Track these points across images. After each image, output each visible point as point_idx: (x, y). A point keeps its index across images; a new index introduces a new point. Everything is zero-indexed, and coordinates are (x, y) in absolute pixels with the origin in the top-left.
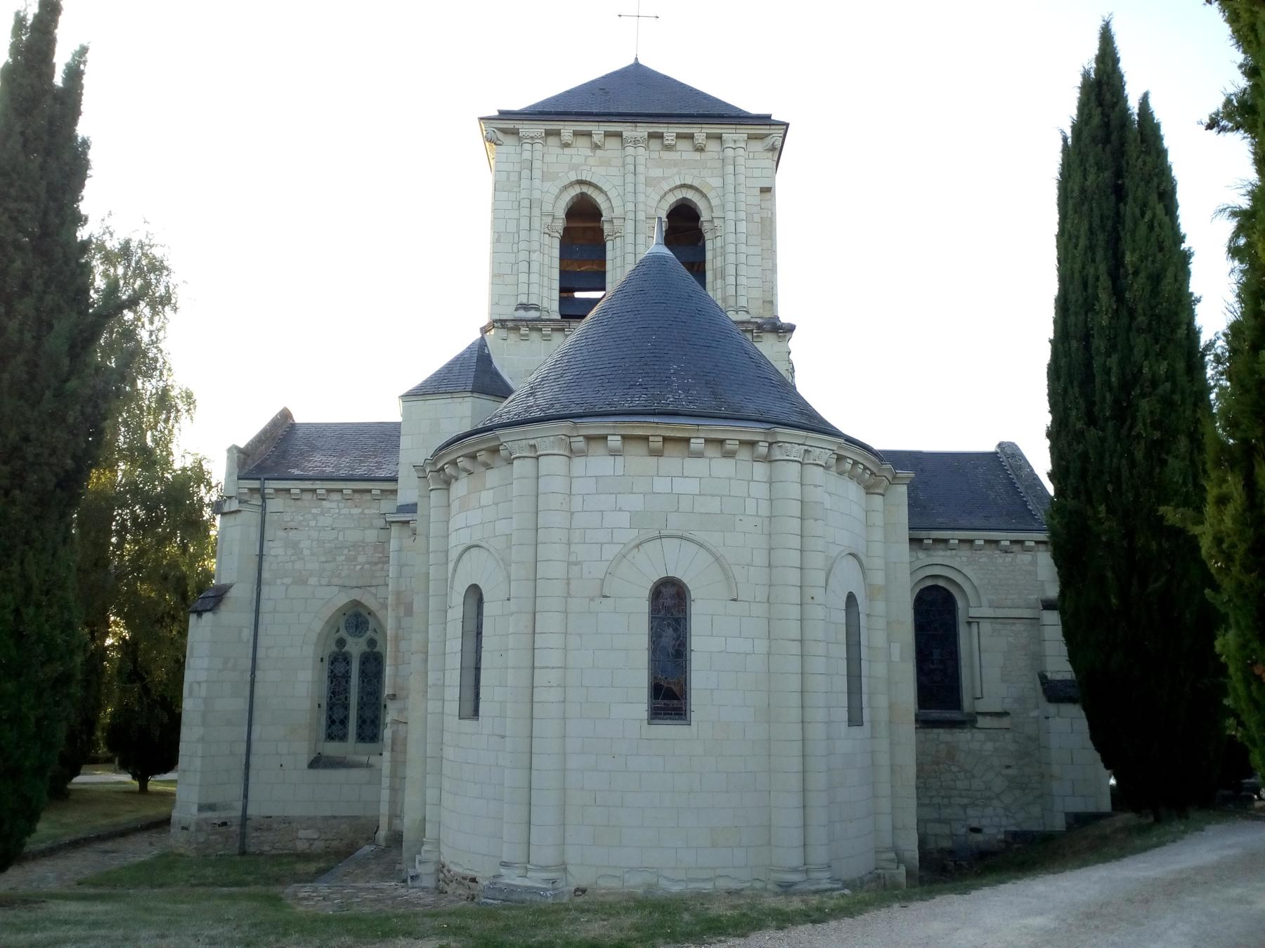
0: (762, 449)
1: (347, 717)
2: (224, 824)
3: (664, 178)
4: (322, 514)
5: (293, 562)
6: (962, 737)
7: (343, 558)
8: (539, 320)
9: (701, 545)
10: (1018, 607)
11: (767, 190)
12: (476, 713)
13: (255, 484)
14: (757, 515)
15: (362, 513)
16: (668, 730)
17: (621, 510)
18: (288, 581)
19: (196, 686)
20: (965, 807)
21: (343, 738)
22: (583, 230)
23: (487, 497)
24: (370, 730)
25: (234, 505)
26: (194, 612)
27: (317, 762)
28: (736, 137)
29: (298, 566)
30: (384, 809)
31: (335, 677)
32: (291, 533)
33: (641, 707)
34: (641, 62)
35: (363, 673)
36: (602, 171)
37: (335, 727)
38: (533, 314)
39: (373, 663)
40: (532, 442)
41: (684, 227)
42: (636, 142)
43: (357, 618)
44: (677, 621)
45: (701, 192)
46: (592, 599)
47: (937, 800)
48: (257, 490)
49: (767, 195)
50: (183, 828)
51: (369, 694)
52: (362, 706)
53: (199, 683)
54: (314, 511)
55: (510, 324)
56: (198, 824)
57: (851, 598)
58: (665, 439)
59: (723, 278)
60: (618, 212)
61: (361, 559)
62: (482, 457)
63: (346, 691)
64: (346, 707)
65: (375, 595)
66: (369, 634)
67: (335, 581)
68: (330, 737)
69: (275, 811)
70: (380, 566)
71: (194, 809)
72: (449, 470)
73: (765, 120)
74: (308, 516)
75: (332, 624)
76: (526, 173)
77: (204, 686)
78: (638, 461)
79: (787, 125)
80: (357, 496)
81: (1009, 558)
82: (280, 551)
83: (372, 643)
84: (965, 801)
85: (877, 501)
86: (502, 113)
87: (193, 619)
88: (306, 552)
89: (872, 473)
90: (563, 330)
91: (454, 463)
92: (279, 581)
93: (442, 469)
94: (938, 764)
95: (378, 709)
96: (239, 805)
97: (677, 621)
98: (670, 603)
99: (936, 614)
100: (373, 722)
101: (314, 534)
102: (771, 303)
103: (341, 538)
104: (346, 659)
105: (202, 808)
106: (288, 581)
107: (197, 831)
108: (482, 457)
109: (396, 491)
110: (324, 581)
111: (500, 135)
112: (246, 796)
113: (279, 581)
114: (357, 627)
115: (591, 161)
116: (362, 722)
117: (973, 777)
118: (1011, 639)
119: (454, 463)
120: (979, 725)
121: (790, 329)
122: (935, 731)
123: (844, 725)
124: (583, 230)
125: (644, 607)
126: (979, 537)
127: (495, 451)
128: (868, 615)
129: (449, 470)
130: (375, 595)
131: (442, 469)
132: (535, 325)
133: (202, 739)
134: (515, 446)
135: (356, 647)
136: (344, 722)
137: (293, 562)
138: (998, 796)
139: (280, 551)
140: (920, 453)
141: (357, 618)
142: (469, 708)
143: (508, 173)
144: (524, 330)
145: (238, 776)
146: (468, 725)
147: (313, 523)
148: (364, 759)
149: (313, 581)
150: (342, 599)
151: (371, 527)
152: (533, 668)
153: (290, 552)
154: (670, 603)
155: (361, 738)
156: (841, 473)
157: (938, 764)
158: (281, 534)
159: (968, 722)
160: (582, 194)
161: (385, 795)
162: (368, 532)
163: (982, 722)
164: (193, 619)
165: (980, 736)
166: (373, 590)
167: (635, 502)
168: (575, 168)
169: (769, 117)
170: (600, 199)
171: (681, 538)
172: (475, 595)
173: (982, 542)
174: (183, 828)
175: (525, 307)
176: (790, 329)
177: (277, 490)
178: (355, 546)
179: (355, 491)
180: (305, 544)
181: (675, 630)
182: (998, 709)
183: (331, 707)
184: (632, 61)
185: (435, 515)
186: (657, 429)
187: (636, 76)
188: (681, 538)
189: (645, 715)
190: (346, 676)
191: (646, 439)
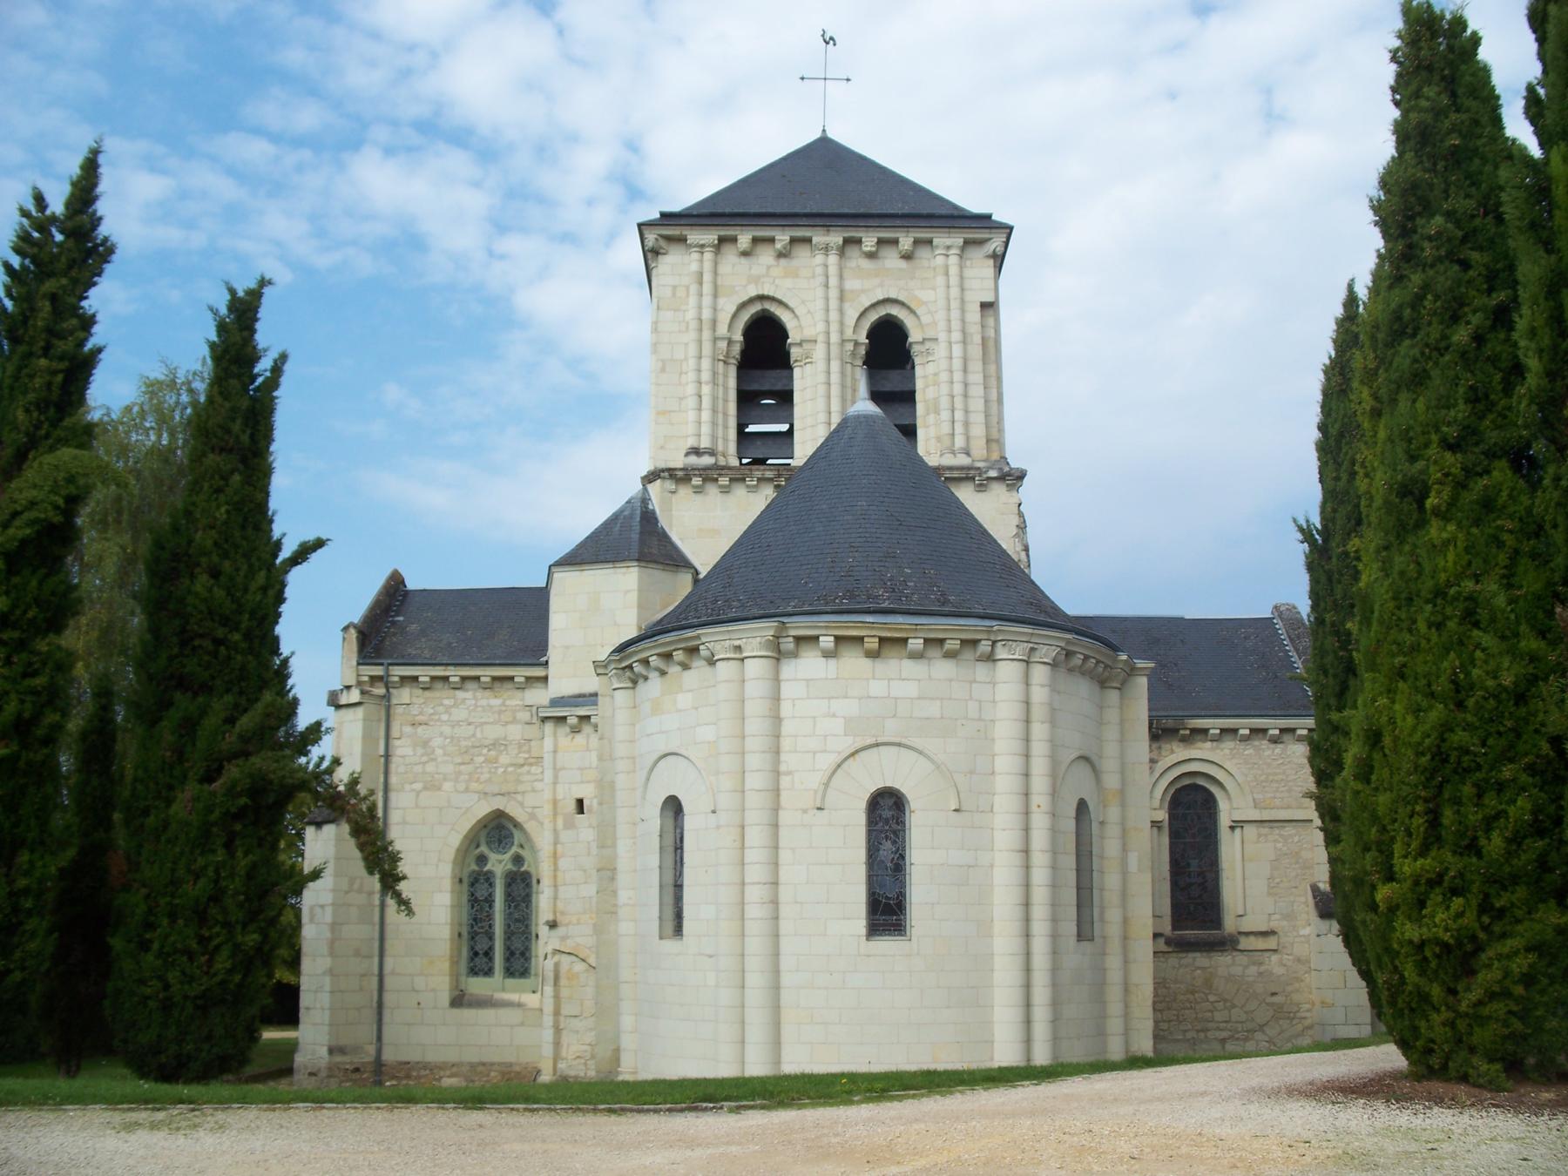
0: (984, 647)
1: (491, 948)
2: (357, 1070)
3: (863, 291)
4: (455, 705)
5: (424, 763)
6: (1222, 962)
7: (482, 759)
8: (716, 467)
9: (921, 753)
10: (1289, 807)
11: (988, 307)
12: (678, 930)
13: (378, 671)
14: (980, 719)
15: (503, 704)
16: (886, 945)
17: (834, 715)
18: (418, 786)
19: (318, 910)
20: (1223, 1041)
21: (489, 972)
22: (764, 350)
23: (684, 700)
24: (519, 963)
25: (355, 696)
26: (310, 823)
27: (459, 1000)
28: (948, 242)
29: (430, 768)
30: (548, 1050)
31: (476, 900)
32: (420, 729)
33: (861, 925)
34: (830, 135)
35: (509, 897)
36: (788, 283)
37: (478, 961)
38: (707, 460)
39: (521, 885)
40: (737, 643)
41: (887, 350)
42: (826, 249)
43: (498, 829)
44: (895, 833)
45: (908, 308)
46: (805, 811)
47: (1189, 1035)
48: (380, 678)
49: (991, 312)
50: (311, 1074)
51: (517, 920)
52: (509, 935)
53: (322, 907)
54: (446, 702)
55: (680, 474)
56: (330, 1069)
57: (1082, 806)
58: (882, 640)
59: (937, 412)
60: (809, 333)
61: (504, 759)
62: (679, 656)
63: (490, 917)
64: (491, 937)
65: (522, 804)
66: (514, 849)
67: (474, 786)
68: (473, 972)
69: (413, 1056)
70: (526, 768)
71: (324, 1051)
72: (638, 668)
73: (984, 221)
74: (441, 709)
75: (472, 840)
76: (694, 288)
77: (329, 910)
78: (853, 663)
79: (1011, 228)
80: (497, 684)
81: (1278, 749)
82: (408, 751)
83: (518, 860)
84: (1225, 1034)
85: (1113, 696)
86: (664, 215)
87: (310, 832)
88: (439, 752)
89: (1106, 666)
90: (743, 480)
91: (646, 662)
92: (407, 787)
93: (630, 667)
94: (1193, 993)
95: (528, 939)
96: (372, 1049)
97: (895, 833)
98: (887, 812)
99: (1192, 816)
100: (523, 954)
101: (447, 730)
102: (994, 440)
103: (479, 735)
104: (489, 878)
105: (331, 1051)
106: (418, 786)
107: (329, 1077)
108: (679, 656)
109: (546, 679)
110: (462, 787)
111: (662, 243)
112: (379, 1038)
113: (407, 787)
114: (500, 842)
115: (775, 272)
116: (510, 954)
117: (1234, 1006)
118: (1279, 845)
119: (646, 662)
120: (1241, 947)
121: (1021, 476)
122: (1191, 955)
123: (1073, 939)
124: (764, 350)
125: (861, 818)
126: (1244, 725)
127: (693, 651)
128: (1102, 823)
129: (638, 668)
130: (522, 804)
131: (630, 667)
132: (709, 475)
133: (331, 972)
134: (718, 647)
135: (499, 864)
136: (489, 954)
137: (424, 763)
138: (1261, 1027)
139: (408, 751)
140: (1179, 621)
141: (498, 829)
142: (670, 926)
143: (675, 287)
144: (696, 481)
145: (369, 1014)
146: (671, 945)
147: (445, 717)
148: (514, 997)
149: (448, 786)
150: (483, 809)
151: (514, 721)
152: (743, 884)
153: (420, 751)
154: (887, 812)
155: (510, 972)
156: (1070, 670)
157: (1193, 993)
158: (408, 729)
159: (1226, 944)
160: (764, 310)
161: (548, 1035)
162: (511, 728)
163: (1245, 943)
164: (310, 832)
165: (1242, 959)
166: (519, 797)
167: (849, 707)
168: (756, 280)
169: (989, 217)
170: (784, 317)
171: (899, 745)
172: (674, 807)
173: (1247, 732)
174: (311, 1074)
175: (696, 451)
176: (1021, 476)
177: (403, 678)
178: (495, 745)
179: (495, 679)
180: (437, 742)
181: (894, 842)
182: (1264, 929)
183: (473, 937)
184: (818, 135)
185: (621, 716)
186: (870, 627)
187: (824, 156)
188: (899, 745)
189: (864, 931)
190: (490, 901)
191: (861, 639)
